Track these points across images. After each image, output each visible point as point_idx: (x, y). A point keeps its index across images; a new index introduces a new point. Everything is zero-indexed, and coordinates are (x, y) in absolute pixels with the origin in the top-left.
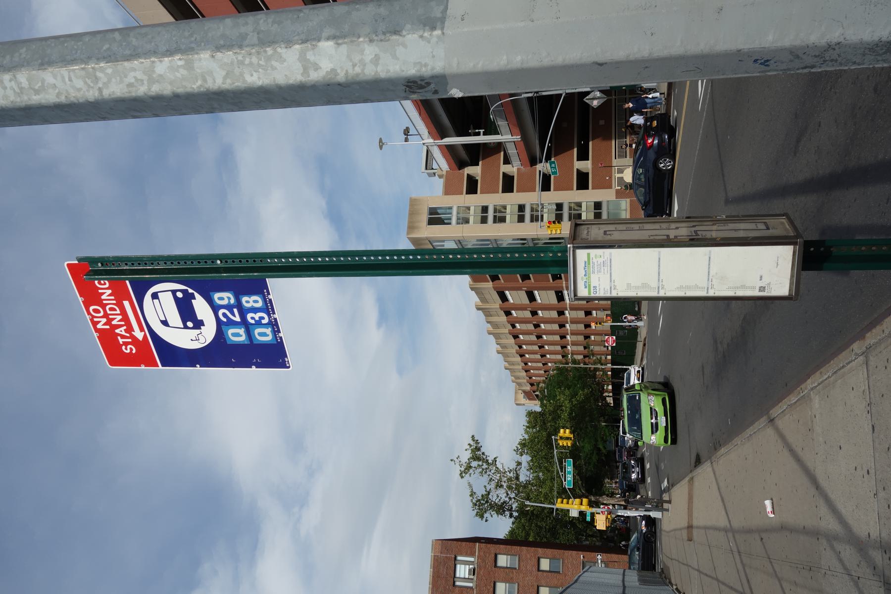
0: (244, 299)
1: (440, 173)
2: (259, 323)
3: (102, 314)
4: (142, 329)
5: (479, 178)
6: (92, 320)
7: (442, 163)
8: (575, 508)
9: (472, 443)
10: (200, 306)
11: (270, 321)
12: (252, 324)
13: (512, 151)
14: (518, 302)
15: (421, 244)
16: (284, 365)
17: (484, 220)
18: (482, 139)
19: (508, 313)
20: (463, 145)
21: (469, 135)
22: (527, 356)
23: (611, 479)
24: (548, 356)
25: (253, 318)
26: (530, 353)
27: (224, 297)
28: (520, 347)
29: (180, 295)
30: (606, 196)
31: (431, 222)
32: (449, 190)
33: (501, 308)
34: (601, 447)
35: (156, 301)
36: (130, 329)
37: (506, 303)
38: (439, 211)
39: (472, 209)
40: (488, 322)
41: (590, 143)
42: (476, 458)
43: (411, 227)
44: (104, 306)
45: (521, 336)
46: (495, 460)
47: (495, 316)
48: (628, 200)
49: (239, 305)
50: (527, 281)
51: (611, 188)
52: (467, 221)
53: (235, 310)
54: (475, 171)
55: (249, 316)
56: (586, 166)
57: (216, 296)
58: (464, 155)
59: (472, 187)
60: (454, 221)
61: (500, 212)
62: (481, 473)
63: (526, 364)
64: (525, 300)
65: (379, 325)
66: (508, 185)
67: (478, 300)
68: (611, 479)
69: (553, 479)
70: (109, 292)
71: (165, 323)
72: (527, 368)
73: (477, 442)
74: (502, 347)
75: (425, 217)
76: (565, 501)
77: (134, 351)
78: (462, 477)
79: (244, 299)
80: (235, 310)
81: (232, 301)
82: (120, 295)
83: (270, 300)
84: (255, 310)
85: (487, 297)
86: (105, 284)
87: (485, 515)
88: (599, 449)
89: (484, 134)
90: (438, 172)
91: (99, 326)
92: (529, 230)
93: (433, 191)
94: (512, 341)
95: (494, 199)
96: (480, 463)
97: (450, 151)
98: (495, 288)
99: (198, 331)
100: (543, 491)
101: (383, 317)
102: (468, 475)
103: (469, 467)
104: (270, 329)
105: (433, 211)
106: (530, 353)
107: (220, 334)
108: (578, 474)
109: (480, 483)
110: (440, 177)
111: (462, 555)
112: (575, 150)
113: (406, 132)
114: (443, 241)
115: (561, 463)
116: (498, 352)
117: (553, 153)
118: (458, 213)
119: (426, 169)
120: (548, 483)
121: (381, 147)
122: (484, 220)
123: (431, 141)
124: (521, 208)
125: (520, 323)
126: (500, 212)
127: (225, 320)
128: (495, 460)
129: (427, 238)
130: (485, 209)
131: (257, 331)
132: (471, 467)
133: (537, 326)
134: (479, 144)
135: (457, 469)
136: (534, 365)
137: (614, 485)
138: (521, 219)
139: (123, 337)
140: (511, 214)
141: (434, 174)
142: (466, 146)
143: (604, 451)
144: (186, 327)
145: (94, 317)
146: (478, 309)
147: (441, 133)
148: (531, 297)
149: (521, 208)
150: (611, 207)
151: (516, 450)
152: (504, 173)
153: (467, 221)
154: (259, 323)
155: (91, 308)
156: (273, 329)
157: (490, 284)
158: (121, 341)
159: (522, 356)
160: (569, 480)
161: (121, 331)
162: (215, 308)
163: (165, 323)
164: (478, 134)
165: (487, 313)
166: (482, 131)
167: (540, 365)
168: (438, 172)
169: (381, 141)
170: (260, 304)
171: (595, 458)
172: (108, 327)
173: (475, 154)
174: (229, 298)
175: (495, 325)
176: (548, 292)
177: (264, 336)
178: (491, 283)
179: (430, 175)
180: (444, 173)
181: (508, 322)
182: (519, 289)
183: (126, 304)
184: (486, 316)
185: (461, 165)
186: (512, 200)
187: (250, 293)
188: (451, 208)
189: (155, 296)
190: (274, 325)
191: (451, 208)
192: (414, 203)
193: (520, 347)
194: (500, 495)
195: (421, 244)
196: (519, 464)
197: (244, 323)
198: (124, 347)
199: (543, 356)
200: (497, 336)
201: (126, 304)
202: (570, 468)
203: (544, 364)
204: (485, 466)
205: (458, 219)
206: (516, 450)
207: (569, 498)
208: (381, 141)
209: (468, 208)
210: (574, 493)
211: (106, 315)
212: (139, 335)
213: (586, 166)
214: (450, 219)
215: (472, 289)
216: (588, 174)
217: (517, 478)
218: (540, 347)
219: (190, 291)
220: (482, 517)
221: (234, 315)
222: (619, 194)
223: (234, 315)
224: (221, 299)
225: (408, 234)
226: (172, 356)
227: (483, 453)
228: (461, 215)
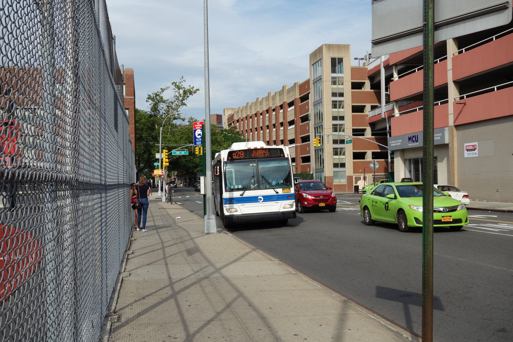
1: (366, 64)
5: (363, 90)
8: (162, 156)
9: (194, 89)
13: (377, 112)
14: (288, 114)
15: (319, 53)
17: (334, 95)
19: (281, 107)
22: (267, 115)
23: (177, 176)
24: (268, 131)
26: (270, 117)
28: (274, 110)
30: (349, 170)
31: (333, 60)
32: (354, 70)
33: (284, 103)
34: (198, 169)
37: (287, 106)
40: (276, 93)
41: (383, 160)
42: (185, 92)
43: (330, 47)
45: (282, 111)
46: (185, 104)
47: (280, 98)
48: (346, 183)
50: (300, 121)
51: (354, 173)
52: (334, 83)
54: (367, 87)
56: (369, 157)
58: (376, 80)
59: (357, 86)
60: (334, 75)
61: (340, 105)
62: (176, 96)
63: (261, 114)
64: (289, 119)
66: (357, 109)
68: (177, 176)
69: (176, 142)
72: (259, 115)
73: (195, 92)
74: (261, 101)
75: (337, 55)
76: (167, 154)
78: (172, 84)
87: (150, 100)
88: (197, 167)
92: (328, 123)
94: (265, 109)
95: (348, 101)
96: (182, 95)
98: (296, 99)
100: (168, 136)
102: (174, 87)
103: (179, 88)
105: (341, 60)
106: (270, 117)
108: (177, 158)
109: (169, 95)
111: (126, 88)
112: (379, 151)
115: (186, 148)
116: (257, 99)
117: (378, 137)
120: (173, 139)
122: (334, 95)
123: (383, 61)
124: (342, 118)
125: (276, 114)
126: (340, 105)
128: (185, 104)
129: (322, 57)
132: (179, 89)
133: (282, 124)
134: (380, 89)
135: (177, 81)
136: (261, 120)
137: (173, 177)
138: (335, 118)
140: (337, 112)
142: (379, 83)
143: (196, 171)
148: (291, 123)
149: (342, 118)
150: (342, 173)
151: (191, 118)
152: (365, 106)
153: (334, 83)
157: (298, 96)
159: (267, 111)
160: (176, 153)
165: (281, 93)
167: (261, 125)
171: (190, 165)
175: (274, 98)
176: (294, 134)
178: (299, 97)
180: (366, 67)
181: (276, 107)
182: (295, 116)
184: (280, 92)
186: (347, 112)
193: (274, 110)
194: (162, 107)
195: (319, 53)
196: (183, 120)
199: (268, 127)
202: (183, 153)
203: (261, 127)
204: (181, 98)
206: (191, 118)
207: (169, 159)
209: (342, 84)
210: (170, 156)
213: (369, 157)
215: (295, 84)
216: (364, 159)
217: (175, 119)
218: (274, 125)
220: (149, 98)
222: (350, 178)
225: (325, 45)
227: (188, 97)
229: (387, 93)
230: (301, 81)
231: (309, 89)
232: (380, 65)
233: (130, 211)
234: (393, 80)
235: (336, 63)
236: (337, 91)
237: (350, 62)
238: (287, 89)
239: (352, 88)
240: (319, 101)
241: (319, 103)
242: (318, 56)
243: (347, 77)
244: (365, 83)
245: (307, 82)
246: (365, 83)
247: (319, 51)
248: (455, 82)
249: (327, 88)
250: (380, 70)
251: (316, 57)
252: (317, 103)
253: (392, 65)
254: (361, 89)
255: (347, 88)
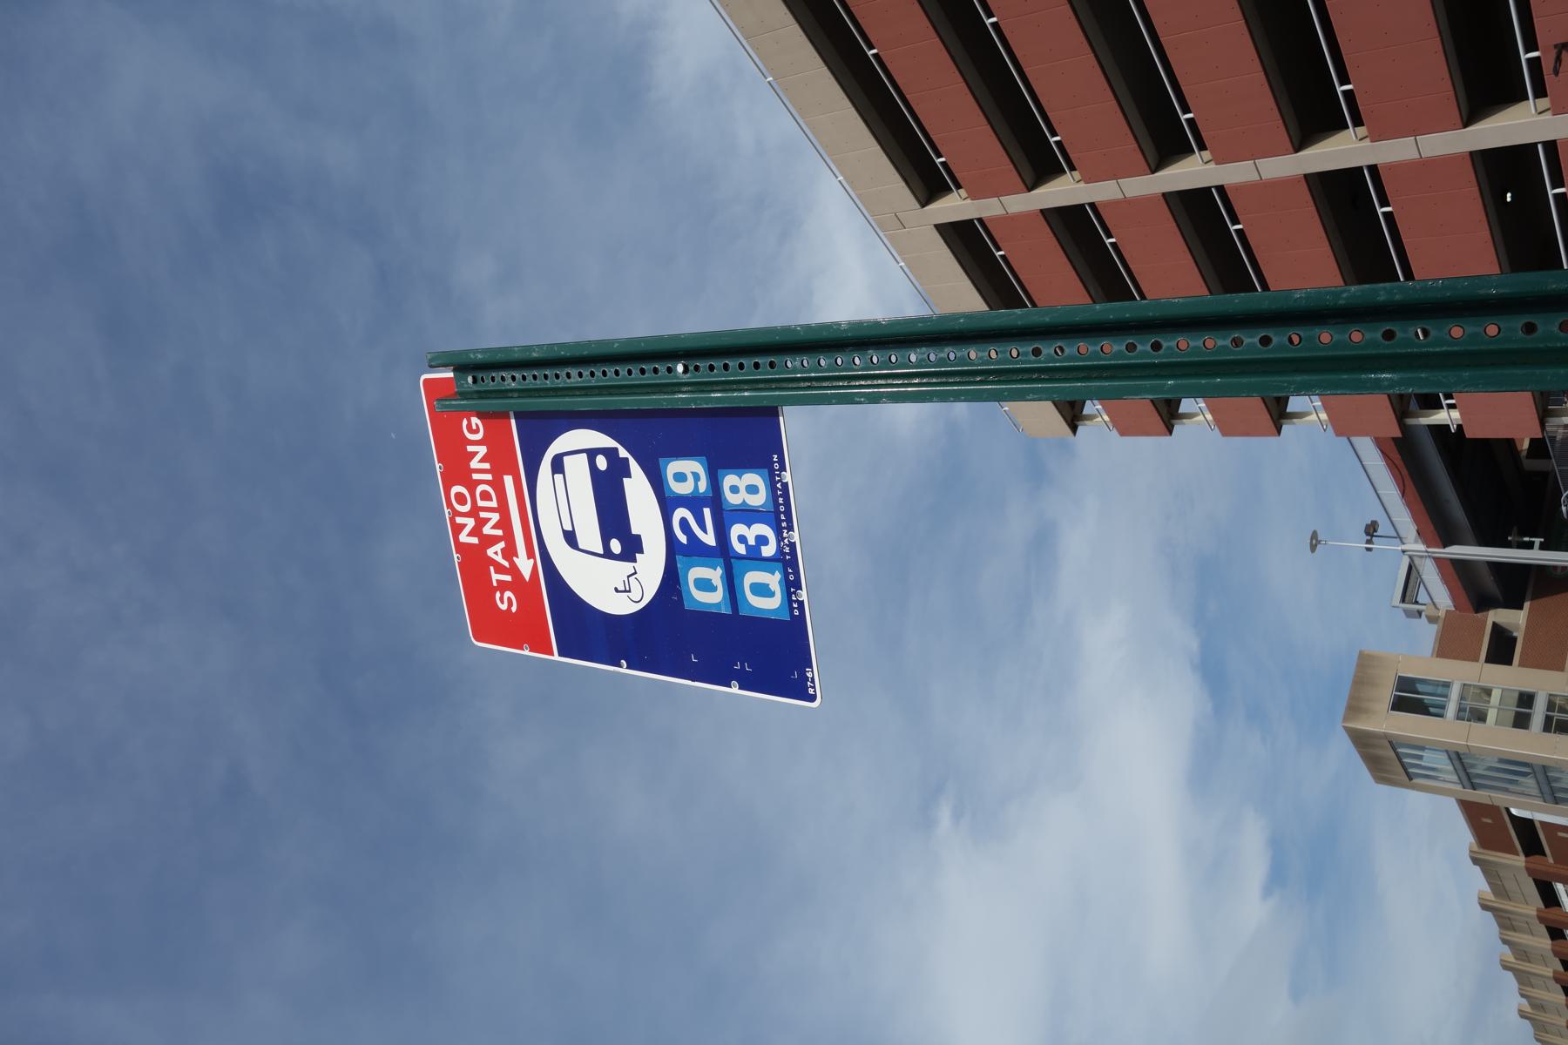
0: (729, 480)
1: (1433, 612)
2: (754, 557)
3: (466, 508)
4: (530, 555)
5: (1519, 635)
6: (452, 520)
7: (1439, 594)
10: (638, 490)
11: (780, 550)
12: (740, 557)
16: (801, 690)
18: (1536, 556)
20: (1490, 563)
21: (1508, 545)
25: (742, 539)
27: (686, 473)
29: (602, 464)
31: (1400, 705)
32: (1447, 647)
33: (1541, 919)
35: (559, 477)
36: (510, 552)
37: (1554, 910)
38: (1420, 687)
39: (1496, 694)
40: (1505, 942)
43: (1355, 708)
44: (472, 486)
49: (715, 499)
52: (1481, 717)
53: (707, 512)
54: (1516, 619)
55: (737, 530)
57: (674, 467)
58: (1489, 583)
59: (1502, 649)
65: (1267, 891)
67: (1487, 888)
70: (482, 450)
71: (570, 538)
74: (1533, 1006)
75: (1387, 693)
77: (514, 609)
79: (729, 480)
80: (707, 512)
81: (703, 486)
82: (500, 462)
83: (785, 485)
84: (748, 515)
85: (1510, 885)
86: (477, 431)
89: (1543, 547)
90: (1428, 610)
91: (464, 538)
93: (1413, 648)
97: (1460, 573)
99: (627, 567)
101: (1277, 878)
104: (778, 575)
105: (1405, 684)
107: (671, 580)
110: (1432, 620)
113: (1371, 530)
114: (1423, 748)
118: (1462, 698)
119: (1403, 600)
121: (1313, 548)
122: (1521, 721)
123: (1422, 547)
127: (683, 539)
129: (1385, 736)
130: (1526, 700)
131: (752, 577)
139: (500, 569)
141: (1420, 613)
142: (1497, 567)
144: (608, 554)
145: (457, 513)
146: (1485, 907)
147: (1440, 529)
153: (1481, 717)
154: (754, 557)
155: (456, 489)
156: (786, 575)
157: (1520, 861)
158: (495, 577)
161: (495, 552)
162: (668, 504)
163: (570, 538)
164: (1530, 546)
165: (1506, 921)
166: (1538, 541)
168: (1428, 610)
169: (1314, 535)
170: (759, 500)
172: (475, 540)
173: (1514, 585)
174: (696, 477)
175: (1521, 953)
177: (763, 595)
178: (1522, 858)
179: (1408, 614)
180: (1442, 614)
183: (508, 480)
184: (1502, 926)
185: (1482, 603)
187: (741, 464)
188: (1447, 685)
189: (558, 466)
190: (786, 561)
191: (1447, 685)
192: (1365, 666)
197: (723, 550)
198: (498, 595)
200: (1523, 978)
201: (508, 480)
205: (1461, 710)
208: (1314, 535)
209: (1488, 692)
211: (474, 512)
212: (525, 565)
214: (1443, 707)
215: (1475, 861)
219: (623, 453)
221: (704, 530)
223: (704, 530)
224: (680, 477)
225: (1345, 719)
226: (583, 630)
228: (1469, 703)
229: (1537, 545)
230: (1464, 836)
231: (1492, 810)
232: (1438, 561)
233: (1316, 871)
234: (1460, 427)
235: (1410, 698)
236: (1513, 708)
237: (1413, 648)
238: (1492, 897)
239: (1509, 662)
240: (1541, 777)
241: (1549, 780)
242: (1381, 752)
243: (1465, 673)
244: (1495, 624)
245: (1474, 813)
246: (1495, 624)
247: (1363, 742)
248: (1469, 119)
249: (1495, 739)
250: (1452, 561)
251: (1387, 762)
252: (1546, 789)
253: (1403, 427)
254: (1515, 639)
255: (1506, 680)
